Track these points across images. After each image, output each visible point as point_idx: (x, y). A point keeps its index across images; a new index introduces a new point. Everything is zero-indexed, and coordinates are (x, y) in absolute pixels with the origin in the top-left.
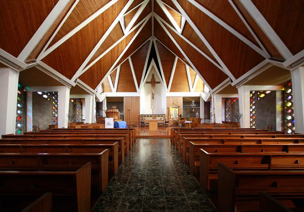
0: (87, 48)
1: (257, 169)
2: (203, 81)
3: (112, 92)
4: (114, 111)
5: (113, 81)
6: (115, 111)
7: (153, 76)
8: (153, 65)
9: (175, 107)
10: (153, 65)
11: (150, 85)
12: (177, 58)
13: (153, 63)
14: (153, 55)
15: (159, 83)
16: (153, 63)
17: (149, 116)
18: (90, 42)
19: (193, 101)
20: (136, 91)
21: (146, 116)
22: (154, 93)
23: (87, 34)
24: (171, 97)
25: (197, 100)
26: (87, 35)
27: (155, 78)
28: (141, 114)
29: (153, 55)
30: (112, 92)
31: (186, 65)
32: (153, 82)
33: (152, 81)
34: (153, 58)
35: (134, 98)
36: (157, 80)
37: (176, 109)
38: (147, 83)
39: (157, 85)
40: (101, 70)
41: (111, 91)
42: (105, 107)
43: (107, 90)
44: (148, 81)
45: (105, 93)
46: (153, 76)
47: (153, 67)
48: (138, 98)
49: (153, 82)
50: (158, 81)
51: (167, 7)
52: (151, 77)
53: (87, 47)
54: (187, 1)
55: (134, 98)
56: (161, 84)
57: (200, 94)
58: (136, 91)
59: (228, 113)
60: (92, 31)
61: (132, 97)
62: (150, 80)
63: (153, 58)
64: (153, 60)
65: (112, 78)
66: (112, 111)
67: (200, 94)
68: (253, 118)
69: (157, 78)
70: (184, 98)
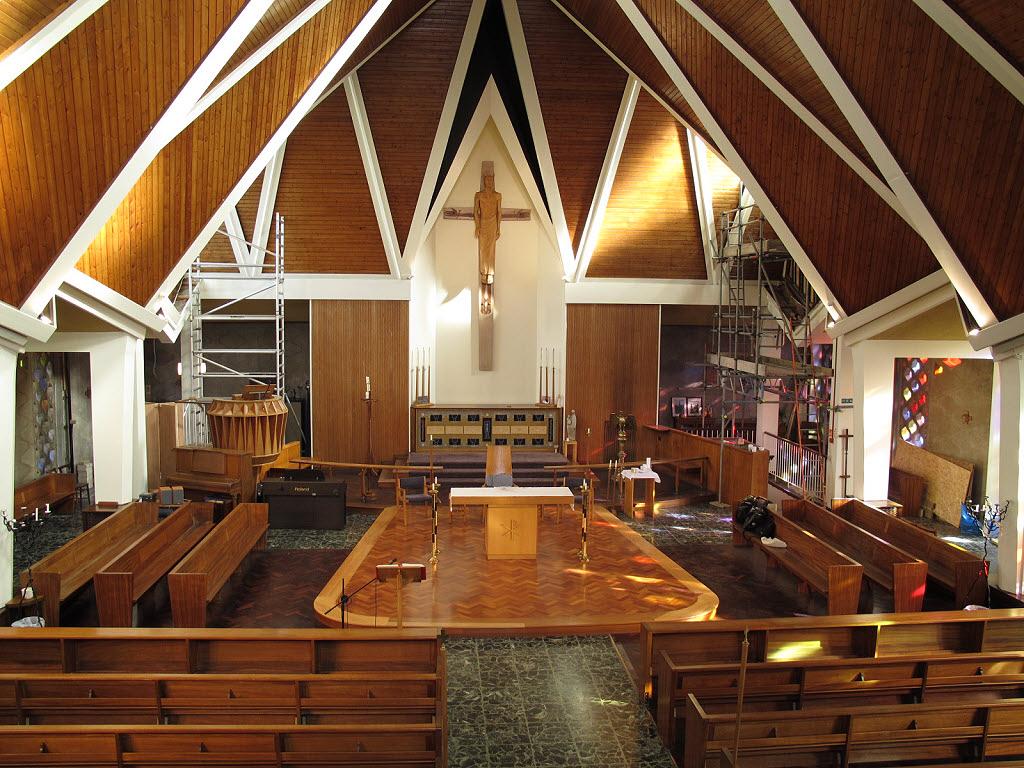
0: (121, 114)
4: (258, 413)
6: (268, 414)
7: (488, 179)
8: (491, 117)
12: (635, 86)
13: (491, 99)
14: (493, 59)
15: (522, 215)
16: (491, 99)
18: (144, 80)
20: (380, 266)
23: (130, 37)
24: (593, 308)
26: (126, 47)
29: (493, 59)
31: (690, 131)
32: (487, 214)
36: (511, 200)
40: (188, 189)
42: (192, 370)
44: (455, 204)
46: (488, 179)
48: (395, 313)
49: (487, 214)
50: (520, 204)
51: (838, 135)
53: (121, 109)
54: (911, 1)
58: (380, 266)
59: (914, 418)
60: (158, 17)
61: (359, 307)
62: (467, 202)
64: (492, 92)
66: (247, 412)
69: (514, 190)
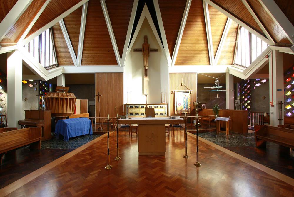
1: (56, 59)
2: (51, 122)
3: (73, 64)
5: (75, 45)
6: (69, 97)
7: (146, 38)
8: (146, 17)
9: (184, 91)
10: (146, 17)
11: (140, 54)
15: (156, 50)
17: (140, 106)
19: (216, 80)
20: (115, 63)
21: (134, 106)
22: (147, 68)
25: (74, 99)
27: (149, 43)
28: (125, 103)
30: (73, 64)
33: (143, 48)
34: (146, 3)
35: (113, 75)
36: (153, 46)
37: (186, 94)
38: (136, 50)
39: (152, 54)
41: (71, 63)
43: (66, 61)
44: (138, 47)
45: (61, 67)
46: (146, 38)
47: (146, 19)
48: (120, 76)
50: (156, 48)
52: (142, 41)
55: (113, 75)
56: (159, 52)
57: (228, 68)
62: (139, 46)
63: (146, 3)
65: (72, 40)
67: (228, 68)
68: (248, 103)
70: (200, 77)
